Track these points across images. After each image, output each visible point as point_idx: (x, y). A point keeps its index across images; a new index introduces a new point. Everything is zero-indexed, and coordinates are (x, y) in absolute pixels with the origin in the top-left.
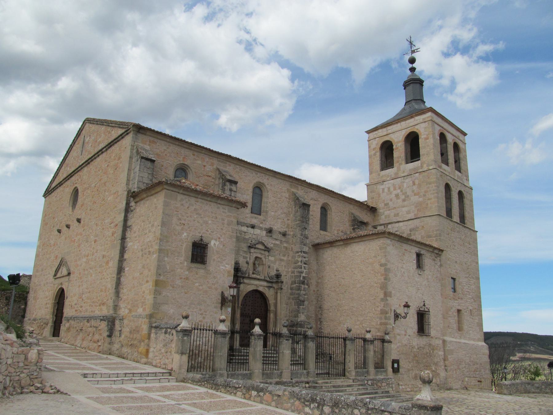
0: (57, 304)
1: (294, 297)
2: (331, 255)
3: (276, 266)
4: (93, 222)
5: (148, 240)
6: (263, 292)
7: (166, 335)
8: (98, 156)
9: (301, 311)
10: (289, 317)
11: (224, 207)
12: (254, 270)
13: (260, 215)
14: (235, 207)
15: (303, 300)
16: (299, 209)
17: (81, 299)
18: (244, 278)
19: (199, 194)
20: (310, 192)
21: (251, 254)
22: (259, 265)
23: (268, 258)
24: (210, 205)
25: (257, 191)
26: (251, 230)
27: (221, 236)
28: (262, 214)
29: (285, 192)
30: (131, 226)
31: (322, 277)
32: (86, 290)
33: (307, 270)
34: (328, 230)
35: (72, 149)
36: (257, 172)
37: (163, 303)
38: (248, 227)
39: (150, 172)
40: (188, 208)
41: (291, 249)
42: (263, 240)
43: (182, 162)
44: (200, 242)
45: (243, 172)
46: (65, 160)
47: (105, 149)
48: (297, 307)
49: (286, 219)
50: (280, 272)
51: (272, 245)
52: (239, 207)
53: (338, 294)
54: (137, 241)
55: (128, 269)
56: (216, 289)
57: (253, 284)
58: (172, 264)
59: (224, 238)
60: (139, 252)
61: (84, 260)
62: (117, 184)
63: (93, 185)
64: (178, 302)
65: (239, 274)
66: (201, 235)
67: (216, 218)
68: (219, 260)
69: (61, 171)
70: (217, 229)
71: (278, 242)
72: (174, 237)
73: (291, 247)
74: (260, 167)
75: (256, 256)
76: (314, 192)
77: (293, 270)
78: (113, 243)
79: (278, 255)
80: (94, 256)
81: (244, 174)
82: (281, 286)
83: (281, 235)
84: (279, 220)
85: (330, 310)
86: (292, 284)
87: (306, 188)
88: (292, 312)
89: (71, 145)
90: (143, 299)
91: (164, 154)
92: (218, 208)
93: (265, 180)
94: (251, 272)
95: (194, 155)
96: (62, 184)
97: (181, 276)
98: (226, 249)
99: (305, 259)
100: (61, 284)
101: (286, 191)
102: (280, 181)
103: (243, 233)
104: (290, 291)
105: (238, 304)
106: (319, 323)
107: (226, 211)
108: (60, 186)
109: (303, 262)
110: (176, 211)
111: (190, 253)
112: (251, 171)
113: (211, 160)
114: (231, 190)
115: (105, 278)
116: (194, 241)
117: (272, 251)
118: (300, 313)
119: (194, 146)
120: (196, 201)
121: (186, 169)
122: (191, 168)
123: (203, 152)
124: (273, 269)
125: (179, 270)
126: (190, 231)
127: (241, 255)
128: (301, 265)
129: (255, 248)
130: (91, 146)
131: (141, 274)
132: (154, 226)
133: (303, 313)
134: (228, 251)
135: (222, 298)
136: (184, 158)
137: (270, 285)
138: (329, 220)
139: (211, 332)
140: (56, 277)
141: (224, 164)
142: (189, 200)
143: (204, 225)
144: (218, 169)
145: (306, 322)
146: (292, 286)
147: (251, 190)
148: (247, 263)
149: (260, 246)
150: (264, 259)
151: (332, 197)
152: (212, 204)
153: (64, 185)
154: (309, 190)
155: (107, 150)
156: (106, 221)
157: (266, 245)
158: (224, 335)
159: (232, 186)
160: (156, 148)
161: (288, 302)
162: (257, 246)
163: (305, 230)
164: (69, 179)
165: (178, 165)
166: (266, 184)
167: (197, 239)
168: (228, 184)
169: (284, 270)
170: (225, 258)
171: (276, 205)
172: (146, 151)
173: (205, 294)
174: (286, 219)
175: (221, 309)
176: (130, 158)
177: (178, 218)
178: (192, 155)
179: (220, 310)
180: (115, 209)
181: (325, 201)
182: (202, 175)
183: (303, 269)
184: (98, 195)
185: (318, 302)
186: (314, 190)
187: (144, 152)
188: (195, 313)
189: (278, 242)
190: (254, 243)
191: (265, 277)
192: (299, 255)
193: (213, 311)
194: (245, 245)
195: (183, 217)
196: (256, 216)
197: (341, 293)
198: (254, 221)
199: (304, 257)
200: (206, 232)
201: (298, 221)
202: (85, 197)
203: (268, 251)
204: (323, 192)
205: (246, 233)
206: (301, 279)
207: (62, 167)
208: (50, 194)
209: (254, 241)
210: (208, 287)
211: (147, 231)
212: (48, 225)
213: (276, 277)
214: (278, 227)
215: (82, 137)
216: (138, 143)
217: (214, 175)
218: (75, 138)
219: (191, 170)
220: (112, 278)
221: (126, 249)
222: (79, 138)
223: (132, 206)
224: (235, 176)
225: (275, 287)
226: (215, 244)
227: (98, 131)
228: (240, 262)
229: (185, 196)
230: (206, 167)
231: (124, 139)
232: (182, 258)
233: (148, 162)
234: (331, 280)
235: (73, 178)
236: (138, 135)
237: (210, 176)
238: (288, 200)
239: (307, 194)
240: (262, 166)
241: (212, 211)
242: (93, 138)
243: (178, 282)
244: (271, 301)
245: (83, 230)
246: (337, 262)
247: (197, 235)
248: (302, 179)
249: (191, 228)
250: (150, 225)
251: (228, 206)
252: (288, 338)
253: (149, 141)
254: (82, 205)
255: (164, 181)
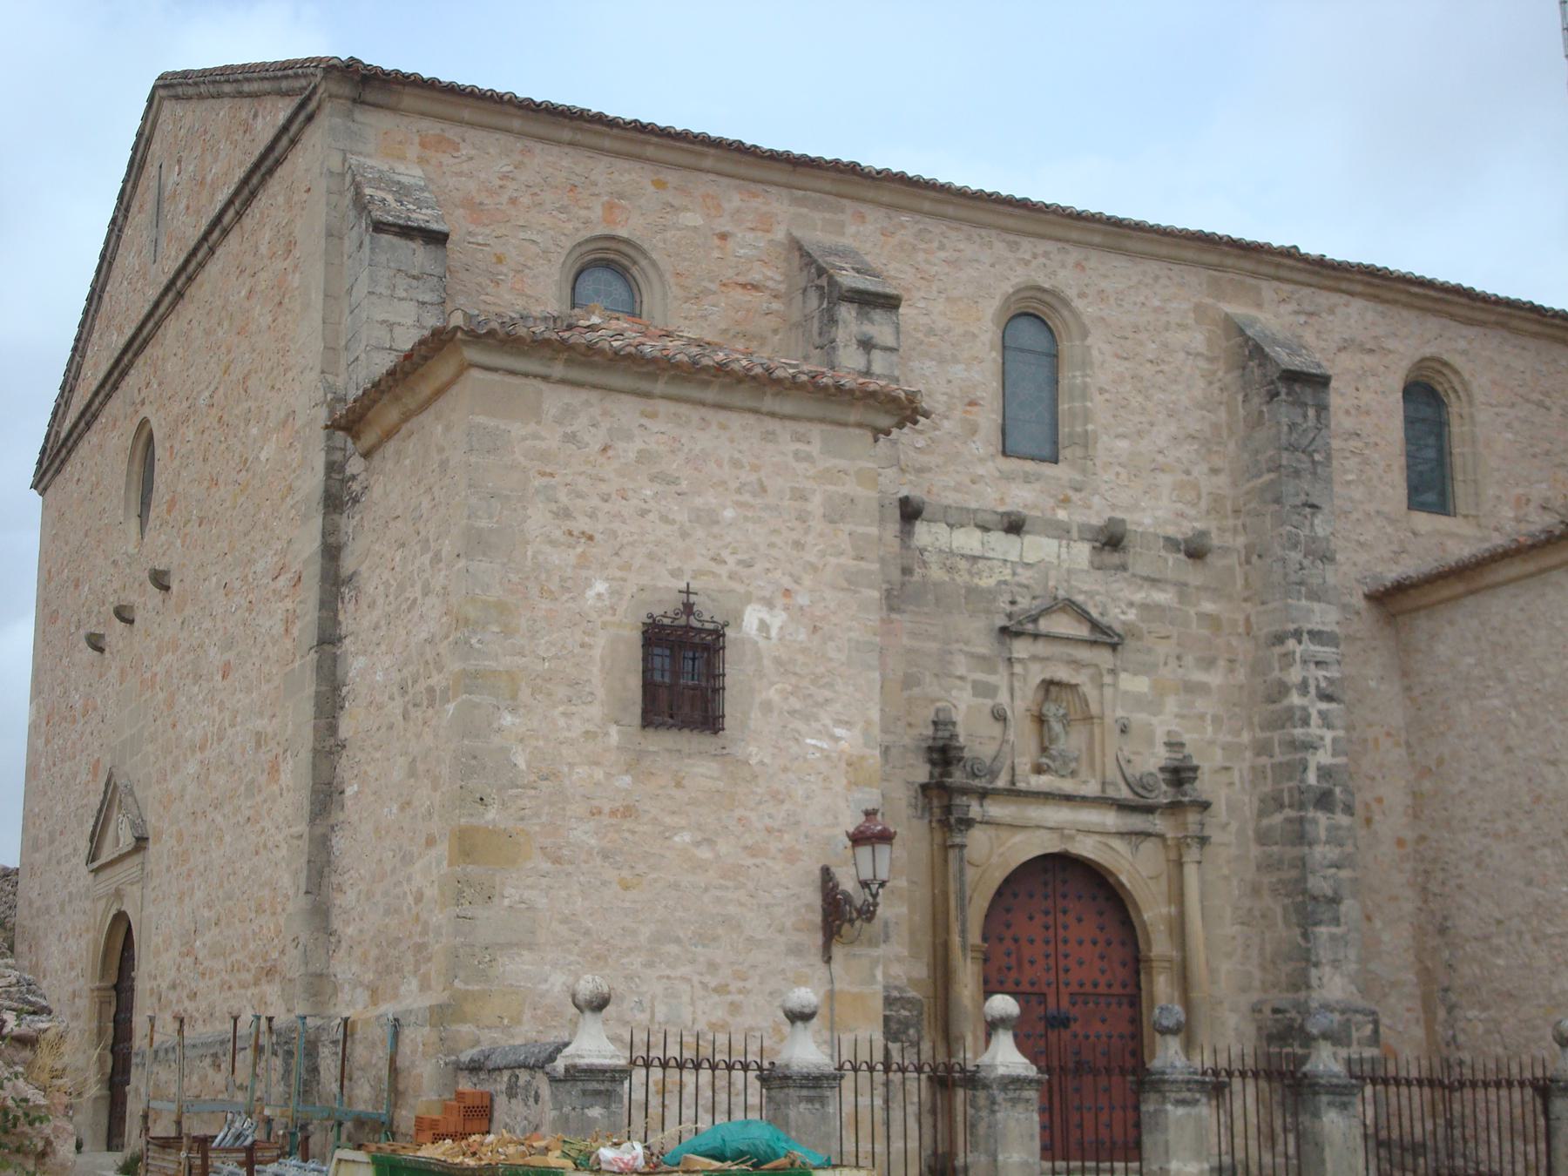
0: (114, 993)
1: (1280, 881)
2: (1477, 639)
3: (1164, 723)
4: (214, 579)
5: (424, 635)
6: (1106, 869)
7: (513, 1101)
8: (212, 251)
9: (1324, 954)
10: (1265, 991)
11: (801, 427)
12: (1044, 750)
13: (1056, 462)
14: (860, 425)
15: (1330, 893)
16: (1265, 409)
17: (189, 960)
18: (983, 794)
19: (653, 377)
20: (1331, 311)
21: (1018, 669)
22: (1066, 721)
23: (1115, 685)
24: (723, 427)
25: (1028, 334)
26: (1002, 544)
27: (797, 581)
28: (1065, 453)
29: (1182, 326)
30: (354, 573)
31: (1440, 762)
32: (206, 913)
33: (1341, 733)
34: (1462, 508)
35: (119, 237)
36: (1011, 238)
37: (510, 945)
38: (985, 529)
39: (427, 298)
40: (604, 450)
41: (1241, 622)
42: (1081, 592)
43: (600, 230)
44: (682, 621)
45: (936, 244)
46: (100, 297)
47: (231, 212)
48: (1298, 931)
49: (1204, 467)
50: (1187, 751)
51: (1132, 615)
52: (884, 421)
53: (1532, 848)
54: (383, 647)
55: (356, 787)
56: (791, 856)
57: (1038, 827)
58: (541, 743)
59: (811, 591)
60: (392, 698)
61: (192, 768)
62: (290, 375)
63: (202, 401)
64: (587, 933)
65: (958, 777)
66: (683, 586)
67: (764, 490)
68: (796, 703)
69: (89, 353)
70: (771, 545)
71: (1163, 597)
72: (544, 605)
73: (1241, 617)
74: (1025, 204)
75: (1047, 676)
76: (1358, 304)
77: (1260, 735)
78: (288, 669)
79: (1173, 663)
80: (225, 744)
81: (942, 254)
82: (1202, 825)
83: (1182, 556)
84: (1166, 480)
85: (1495, 941)
86: (1262, 813)
87: (1308, 291)
88: (1273, 962)
89: (114, 221)
90: (419, 929)
91: (504, 198)
92: (769, 436)
93: (1062, 273)
94: (1024, 764)
95: (660, 185)
96: (95, 417)
97: (596, 803)
98: (831, 644)
99: (1321, 673)
100: (118, 894)
101: (1190, 321)
102: (1153, 267)
103: (963, 565)
104: (1255, 851)
105: (963, 932)
106: (1442, 1014)
107: (815, 449)
108: (88, 426)
109: (1313, 690)
110: (543, 474)
111: (635, 683)
112: (984, 232)
113: (756, 203)
114: (867, 345)
115: (270, 844)
116: (651, 616)
117: (1130, 643)
118: (1316, 965)
119: (655, 139)
120: (644, 414)
121: (626, 263)
122: (654, 256)
123: (708, 163)
124: (1150, 741)
125: (582, 770)
126: (627, 567)
127: (961, 678)
128: (1304, 709)
129: (1036, 636)
130: (188, 208)
131: (406, 805)
132: (441, 561)
133: (1336, 963)
134: (843, 658)
135: (825, 899)
136: (610, 207)
137: (1137, 822)
138: (1459, 450)
139: (738, 1075)
140: (96, 865)
141: (828, 215)
142: (605, 413)
143: (700, 533)
144: (797, 246)
145: (1356, 1011)
146: (1265, 822)
147: (987, 332)
148: (1000, 716)
149: (1062, 625)
150: (1089, 690)
151: (1470, 322)
152: (736, 421)
153: (102, 419)
154: (1325, 299)
155: (239, 215)
156: (260, 566)
157: (1095, 613)
158: (814, 1087)
159: (872, 322)
160: (460, 174)
161: (1250, 910)
162: (1044, 625)
163: (1313, 514)
164: (115, 387)
165: (579, 244)
166: (1071, 293)
167: (665, 606)
168: (846, 312)
169: (1211, 743)
170: (828, 694)
171: (1136, 400)
172: (402, 191)
173: (730, 884)
174: (1200, 470)
175: (828, 960)
176: (329, 234)
177: (554, 507)
178: (651, 188)
179: (819, 964)
180: (289, 501)
181: (1428, 351)
182: (713, 287)
183: (1315, 730)
184: (223, 446)
185: (1425, 901)
186: (1352, 294)
187: (390, 198)
188: (686, 987)
189: (1163, 597)
190: (1024, 611)
191: (1104, 784)
192: (1285, 655)
193: (783, 971)
194: (980, 623)
195: (579, 501)
196: (1030, 466)
197: (1544, 844)
198: (1021, 498)
199: (1318, 663)
200: (713, 564)
201: (1269, 470)
202: (177, 463)
203: (1114, 647)
204: (1403, 298)
205: (981, 564)
206: (1312, 778)
207: (90, 333)
208: (58, 471)
209: (1024, 603)
210: (746, 848)
211: (416, 592)
212: (59, 624)
213: (1169, 783)
214: (1159, 513)
215: (151, 170)
216: (362, 159)
217: (779, 278)
218: (125, 182)
219: (654, 264)
220: (296, 842)
221: (345, 690)
222: (143, 181)
223: (354, 477)
224: (892, 269)
225: (1170, 835)
226: (764, 626)
227: (205, 132)
228: (959, 716)
229: (584, 395)
230: (730, 244)
231: (299, 146)
232: (596, 711)
233: (412, 245)
234: (1489, 776)
235: (132, 380)
236: (358, 116)
237: (755, 287)
238: (1202, 364)
239: (1312, 320)
240: (1035, 198)
241: (737, 455)
242: (191, 168)
243: (583, 834)
244: (1153, 911)
245: (179, 621)
246: (1510, 675)
247: (660, 584)
248: (1275, 244)
249: (626, 554)
250: (426, 558)
251: (822, 420)
252: (1187, 1095)
253: (417, 140)
254: (172, 504)
255: (457, 328)
